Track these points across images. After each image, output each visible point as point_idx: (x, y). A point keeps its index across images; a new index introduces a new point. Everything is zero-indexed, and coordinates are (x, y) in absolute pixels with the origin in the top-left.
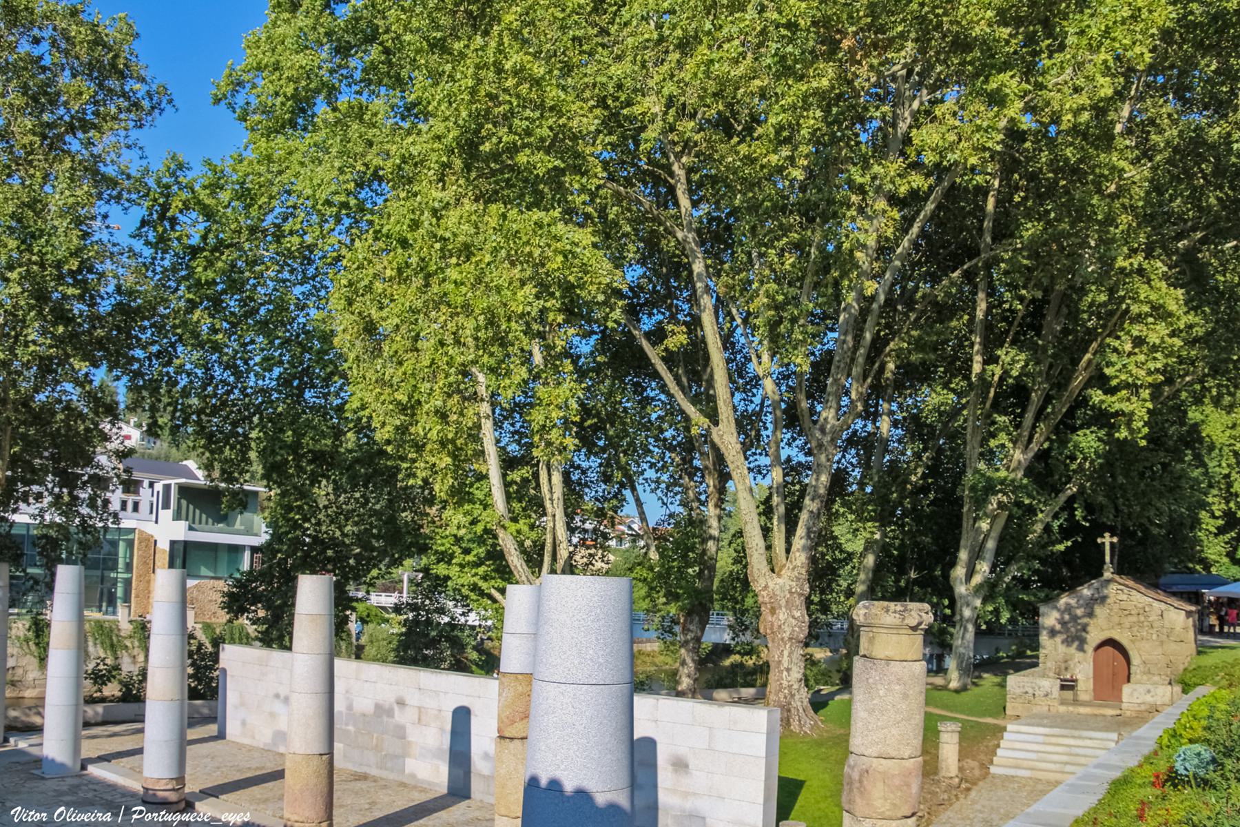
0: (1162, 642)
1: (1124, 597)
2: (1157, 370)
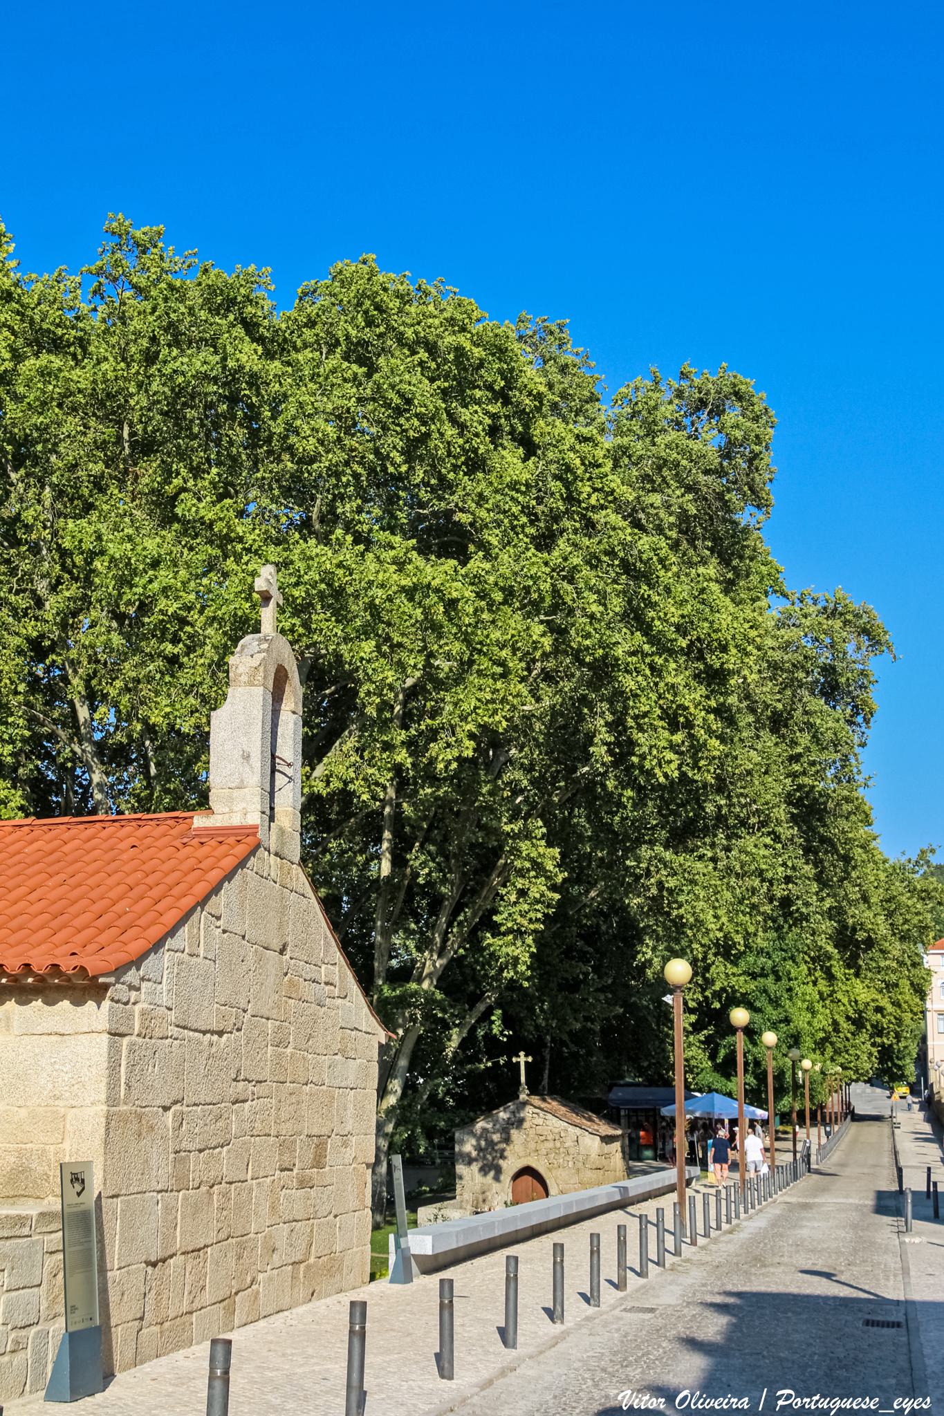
0: (578, 1170)
1: (540, 1121)
2: (537, 920)
